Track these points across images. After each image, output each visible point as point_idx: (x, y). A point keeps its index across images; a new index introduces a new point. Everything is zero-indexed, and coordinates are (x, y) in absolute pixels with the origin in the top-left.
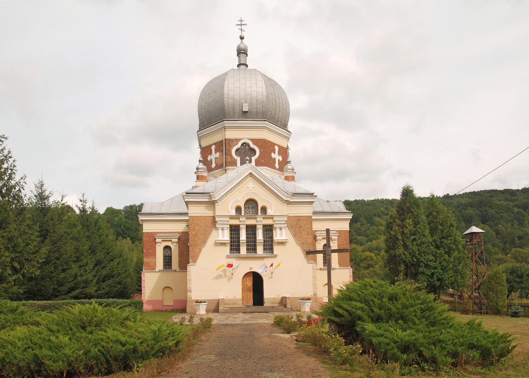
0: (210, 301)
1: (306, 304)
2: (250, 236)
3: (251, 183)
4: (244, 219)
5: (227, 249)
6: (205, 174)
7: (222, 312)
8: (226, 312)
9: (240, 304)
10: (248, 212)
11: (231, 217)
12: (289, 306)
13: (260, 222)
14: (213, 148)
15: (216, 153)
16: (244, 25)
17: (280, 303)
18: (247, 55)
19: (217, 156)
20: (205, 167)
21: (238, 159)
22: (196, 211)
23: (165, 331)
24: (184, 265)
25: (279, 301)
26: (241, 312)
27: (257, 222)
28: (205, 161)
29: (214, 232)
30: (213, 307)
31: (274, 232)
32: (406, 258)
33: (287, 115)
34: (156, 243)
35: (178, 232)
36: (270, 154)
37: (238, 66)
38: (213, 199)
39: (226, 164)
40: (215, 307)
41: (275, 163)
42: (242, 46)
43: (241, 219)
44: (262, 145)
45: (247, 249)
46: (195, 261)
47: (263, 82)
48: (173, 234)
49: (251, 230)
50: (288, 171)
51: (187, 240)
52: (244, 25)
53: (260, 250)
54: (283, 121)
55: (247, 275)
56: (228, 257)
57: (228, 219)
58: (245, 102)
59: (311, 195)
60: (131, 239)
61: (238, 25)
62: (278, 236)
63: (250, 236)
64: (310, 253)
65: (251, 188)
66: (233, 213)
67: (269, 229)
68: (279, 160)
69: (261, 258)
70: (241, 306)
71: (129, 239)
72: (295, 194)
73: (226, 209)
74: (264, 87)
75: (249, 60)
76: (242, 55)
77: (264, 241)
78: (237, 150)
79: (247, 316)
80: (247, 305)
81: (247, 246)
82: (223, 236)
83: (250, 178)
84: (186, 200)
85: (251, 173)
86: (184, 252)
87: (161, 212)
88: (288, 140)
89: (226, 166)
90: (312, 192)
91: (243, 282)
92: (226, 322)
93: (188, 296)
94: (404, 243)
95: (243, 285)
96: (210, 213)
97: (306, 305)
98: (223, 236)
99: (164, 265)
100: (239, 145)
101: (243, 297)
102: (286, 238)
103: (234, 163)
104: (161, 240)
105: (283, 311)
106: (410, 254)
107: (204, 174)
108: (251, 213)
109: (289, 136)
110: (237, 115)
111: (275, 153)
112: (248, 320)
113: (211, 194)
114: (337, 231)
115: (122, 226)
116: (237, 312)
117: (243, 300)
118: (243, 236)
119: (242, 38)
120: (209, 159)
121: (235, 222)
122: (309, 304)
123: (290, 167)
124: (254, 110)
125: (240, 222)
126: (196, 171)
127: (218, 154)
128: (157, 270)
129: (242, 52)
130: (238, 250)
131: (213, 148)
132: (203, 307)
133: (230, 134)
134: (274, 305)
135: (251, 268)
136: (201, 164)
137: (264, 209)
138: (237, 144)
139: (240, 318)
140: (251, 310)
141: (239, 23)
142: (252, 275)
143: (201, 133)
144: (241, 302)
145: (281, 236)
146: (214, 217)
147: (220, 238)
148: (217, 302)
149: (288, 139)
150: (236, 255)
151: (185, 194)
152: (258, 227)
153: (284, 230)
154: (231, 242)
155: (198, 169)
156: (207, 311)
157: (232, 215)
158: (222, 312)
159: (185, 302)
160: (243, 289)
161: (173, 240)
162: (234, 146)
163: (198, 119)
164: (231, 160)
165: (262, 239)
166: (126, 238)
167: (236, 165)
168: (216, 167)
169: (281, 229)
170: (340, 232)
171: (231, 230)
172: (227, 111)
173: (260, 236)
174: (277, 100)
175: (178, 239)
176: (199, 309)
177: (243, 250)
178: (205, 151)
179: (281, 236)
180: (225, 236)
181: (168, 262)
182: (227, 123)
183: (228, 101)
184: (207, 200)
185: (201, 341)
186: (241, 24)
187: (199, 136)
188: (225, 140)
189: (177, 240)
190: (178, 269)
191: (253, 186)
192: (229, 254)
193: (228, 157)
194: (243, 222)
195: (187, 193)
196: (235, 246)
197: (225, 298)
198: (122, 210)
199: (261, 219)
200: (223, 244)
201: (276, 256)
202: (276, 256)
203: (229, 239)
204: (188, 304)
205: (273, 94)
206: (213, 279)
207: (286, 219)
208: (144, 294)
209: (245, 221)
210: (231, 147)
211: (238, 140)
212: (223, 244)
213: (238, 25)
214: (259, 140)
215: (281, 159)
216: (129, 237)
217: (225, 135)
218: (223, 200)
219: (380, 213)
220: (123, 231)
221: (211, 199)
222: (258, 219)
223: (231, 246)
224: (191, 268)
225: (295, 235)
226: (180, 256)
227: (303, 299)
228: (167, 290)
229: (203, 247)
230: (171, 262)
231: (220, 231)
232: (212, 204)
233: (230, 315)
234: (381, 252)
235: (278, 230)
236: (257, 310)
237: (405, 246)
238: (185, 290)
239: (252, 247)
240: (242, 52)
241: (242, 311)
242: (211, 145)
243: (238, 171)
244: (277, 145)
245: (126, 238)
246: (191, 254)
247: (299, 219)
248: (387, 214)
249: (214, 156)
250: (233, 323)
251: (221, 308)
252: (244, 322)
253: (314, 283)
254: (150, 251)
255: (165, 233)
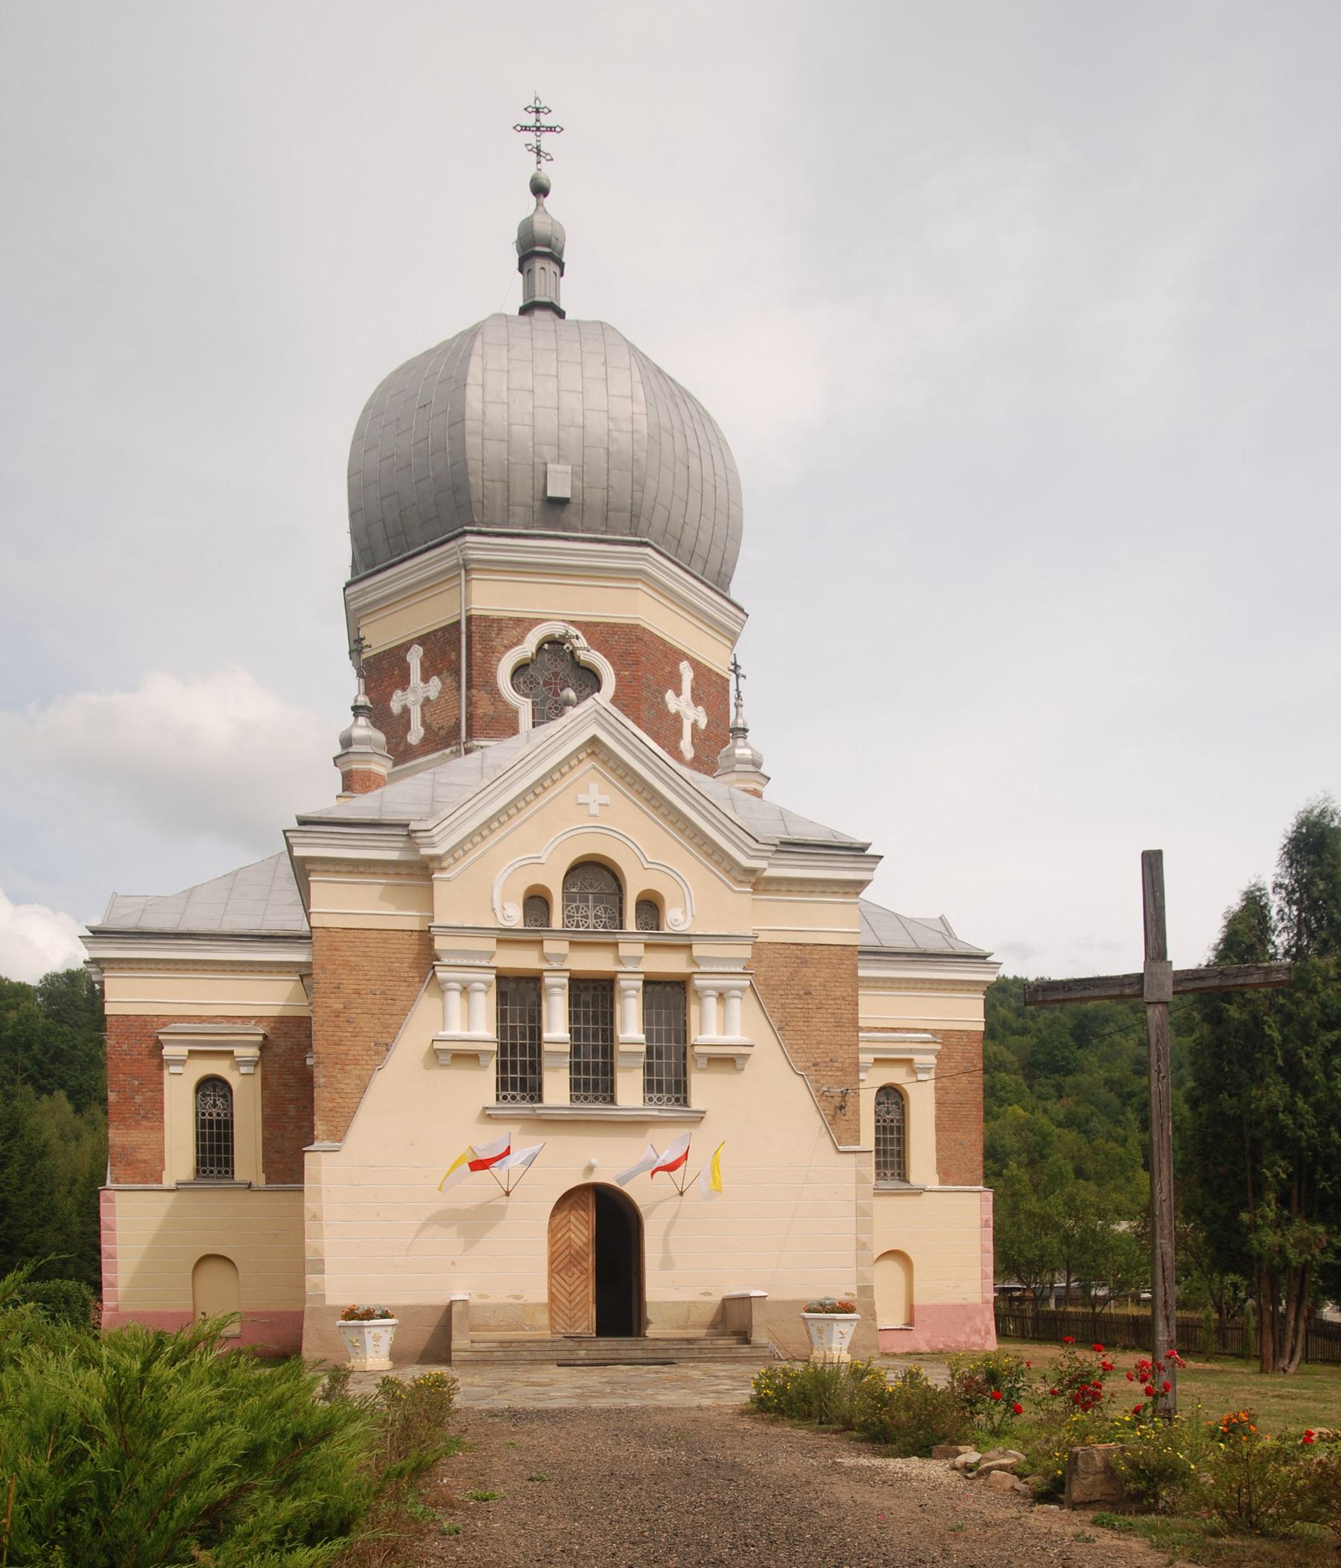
0: (410, 1313)
1: (837, 1328)
2: (590, 1024)
3: (594, 787)
4: (563, 947)
5: (483, 1083)
6: (381, 767)
7: (466, 1362)
8: (482, 1360)
9: (540, 1328)
10: (578, 917)
11: (506, 938)
12: (759, 1337)
13: (632, 961)
14: (415, 657)
15: (425, 679)
16: (551, 129)
17: (713, 1325)
18: (561, 265)
19: (433, 695)
20: (380, 737)
21: (524, 707)
22: (345, 905)
23: (201, 1427)
24: (286, 1167)
25: (708, 1315)
26: (550, 1361)
27: (619, 960)
28: (375, 709)
29: (426, 1005)
30: (421, 1336)
31: (694, 1011)
32: (1301, 1127)
33: (733, 536)
34: (161, 1064)
35: (259, 1019)
36: (662, 695)
37: (525, 310)
38: (424, 851)
39: (469, 727)
40: (437, 1338)
41: (679, 734)
42: (541, 227)
43: (549, 947)
44: (627, 653)
45: (575, 1085)
46: (338, 1134)
47: (637, 377)
48: (239, 1027)
49: (593, 996)
50: (738, 767)
51: (305, 1046)
52: (551, 129)
53: (629, 1088)
54: (714, 565)
55: (570, 1199)
56: (488, 1116)
57: (490, 945)
58: (559, 458)
59: (857, 851)
60: (70, 1097)
61: (525, 128)
62: (711, 1027)
63: (590, 1024)
64: (837, 1109)
65: (594, 809)
66: (514, 916)
67: (669, 996)
68: (695, 725)
69: (635, 1124)
70: (547, 1334)
71: (61, 1095)
72: (790, 847)
73: (483, 896)
74: (641, 396)
75: (573, 292)
76: (538, 263)
77: (649, 1050)
78: (520, 669)
79: (594, 1378)
80: (571, 1332)
81: (575, 1068)
82: (468, 1023)
83: (589, 764)
84: (298, 852)
85: (594, 740)
86: (287, 1099)
87: (182, 929)
88: (733, 643)
89: (470, 735)
90: (859, 837)
91: (552, 1232)
92: (502, 1403)
93: (309, 1290)
94: (1290, 1057)
95: (552, 1243)
96: (409, 919)
97: (836, 1335)
98: (468, 1023)
99: (201, 1162)
100: (528, 647)
101: (552, 1297)
102: (746, 1040)
103: (505, 725)
104: (183, 1050)
105: (735, 1360)
106: (1318, 1107)
107: (374, 767)
108: (591, 921)
109: (736, 628)
110: (519, 511)
111: (678, 694)
112: (602, 1394)
113: (413, 826)
114: (934, 1032)
115: (35, 1048)
116: (533, 1362)
117: (551, 1310)
118: (557, 1025)
119: (540, 190)
120: (395, 706)
121: (523, 960)
122: (849, 1330)
123: (747, 752)
124: (596, 496)
125: (545, 958)
126: (338, 750)
127: (435, 683)
128: (168, 1182)
129: (537, 251)
130: (533, 1090)
131: (415, 657)
132: (377, 1338)
133: (489, 597)
134: (691, 1333)
135: (590, 1169)
136: (362, 720)
137: (651, 907)
138: (520, 641)
139: (561, 1388)
140: (593, 1355)
141: (530, 120)
142: (591, 1202)
143: (364, 593)
144: (544, 1319)
145: (724, 1028)
146: (426, 937)
147: (456, 1029)
148: (436, 1319)
149: (732, 637)
150: (524, 1107)
151: (295, 825)
152: (623, 984)
153: (735, 1005)
154: (503, 1049)
155: (347, 742)
156: (397, 1357)
157: (508, 924)
158: (466, 1362)
159: (295, 1321)
160: (551, 1262)
161: (238, 1051)
162: (508, 648)
163: (347, 539)
164: (491, 710)
165: (642, 1037)
166: (50, 1093)
167: (514, 731)
168: (425, 740)
169: (722, 997)
170: (946, 1036)
171: (502, 997)
172: (476, 494)
173: (631, 1025)
174: (694, 464)
175: (262, 1048)
176: (360, 1347)
177: (556, 1086)
178: (380, 673)
179: (724, 1028)
180: (476, 1021)
181: (215, 1148)
182: (476, 548)
183: (483, 452)
184: (393, 856)
185: (450, 1505)
186: (538, 125)
187: (353, 606)
188: (469, 619)
189: (253, 1052)
190: (260, 1180)
191: (605, 799)
192: (492, 1101)
193: (481, 697)
194: (560, 960)
195: (303, 822)
196: (518, 1070)
197: (475, 1300)
198: (38, 990)
199: (638, 950)
200: (466, 1058)
201: (698, 1118)
202: (699, 1117)
203: (492, 1035)
204: (307, 1323)
205: (677, 434)
206: (419, 1218)
207: (746, 952)
208: (112, 1285)
209: (563, 957)
210: (493, 654)
211: (523, 624)
212: (466, 1058)
213: (525, 128)
214: (613, 628)
215: (703, 723)
216: (62, 1087)
217: (468, 600)
218: (470, 858)
219: (998, 1027)
220: (39, 1064)
221: (417, 851)
222: (624, 950)
223: (502, 1067)
224: (323, 1165)
225: (782, 1029)
226: (268, 1122)
227: (822, 1307)
228: (213, 1273)
229: (377, 1067)
230: (229, 1150)
231: (454, 998)
232: (420, 872)
233: (505, 1372)
234: (1006, 1166)
235: (711, 1003)
236: (623, 1354)
237: (1293, 1073)
238: (297, 1264)
239: (594, 1077)
240: (537, 251)
241: (554, 1355)
242: (405, 647)
243: (534, 746)
244: (687, 657)
245: (50, 1093)
246: (322, 1098)
247: (802, 955)
248: (1024, 1031)
249: (417, 695)
250: (540, 1405)
251: (460, 1342)
252: (595, 1404)
253: (863, 1237)
254: (138, 1099)
255: (200, 1019)
